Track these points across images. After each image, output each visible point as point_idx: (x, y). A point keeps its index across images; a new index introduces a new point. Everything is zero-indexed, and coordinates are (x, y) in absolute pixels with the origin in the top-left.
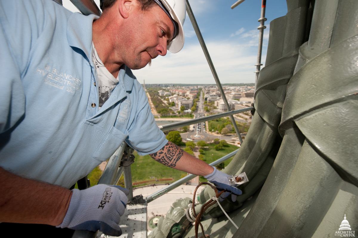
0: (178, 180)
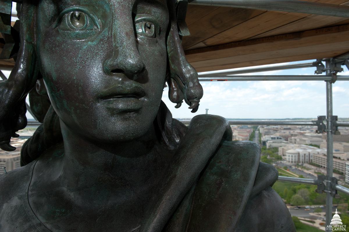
0: (45, 87)
